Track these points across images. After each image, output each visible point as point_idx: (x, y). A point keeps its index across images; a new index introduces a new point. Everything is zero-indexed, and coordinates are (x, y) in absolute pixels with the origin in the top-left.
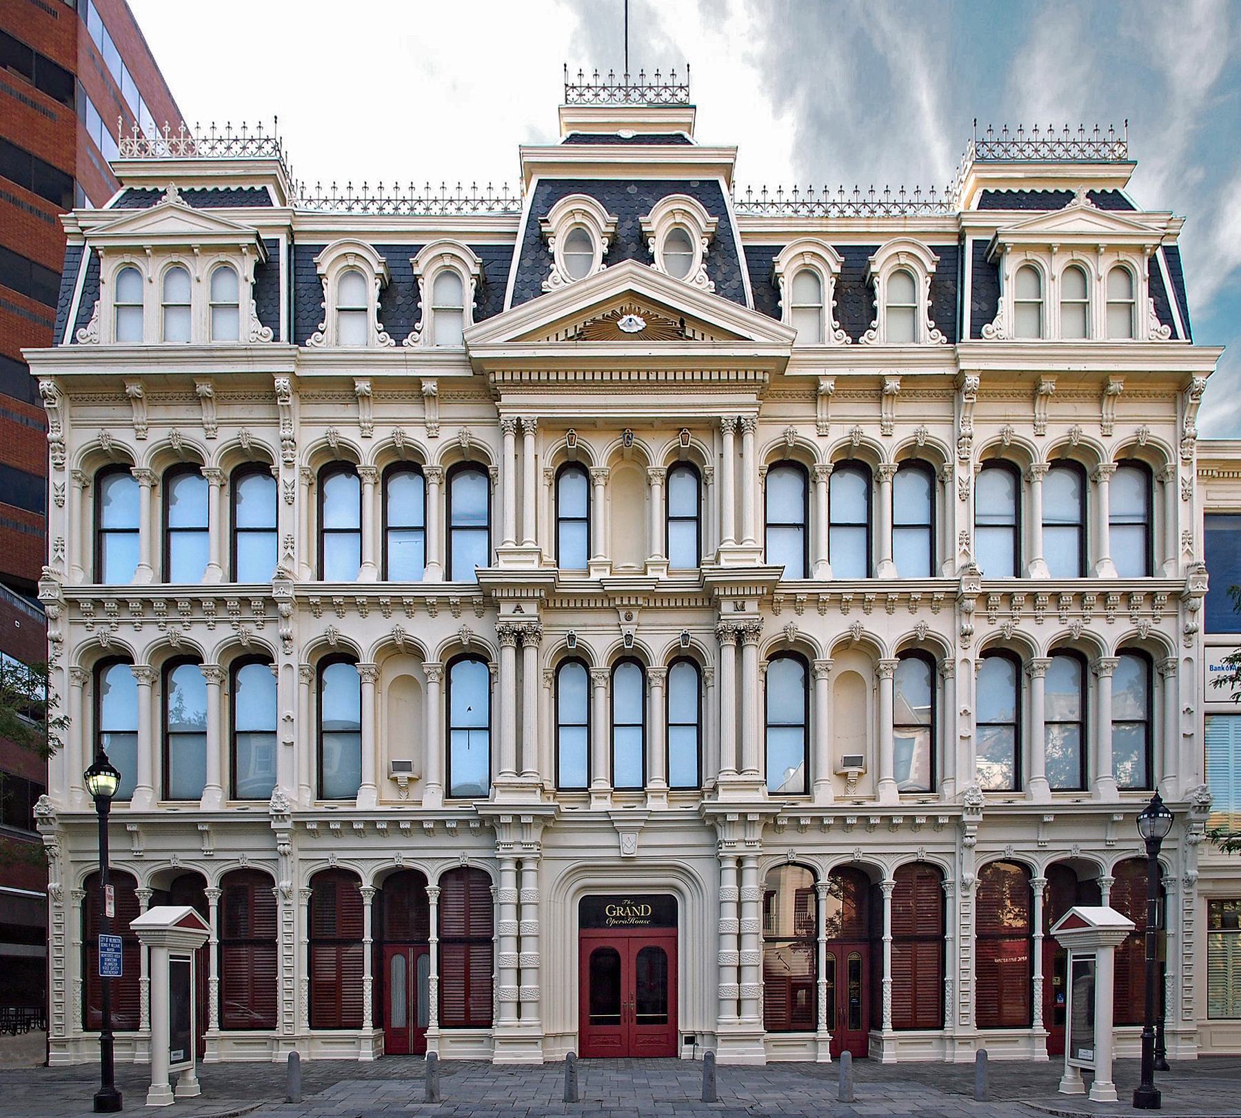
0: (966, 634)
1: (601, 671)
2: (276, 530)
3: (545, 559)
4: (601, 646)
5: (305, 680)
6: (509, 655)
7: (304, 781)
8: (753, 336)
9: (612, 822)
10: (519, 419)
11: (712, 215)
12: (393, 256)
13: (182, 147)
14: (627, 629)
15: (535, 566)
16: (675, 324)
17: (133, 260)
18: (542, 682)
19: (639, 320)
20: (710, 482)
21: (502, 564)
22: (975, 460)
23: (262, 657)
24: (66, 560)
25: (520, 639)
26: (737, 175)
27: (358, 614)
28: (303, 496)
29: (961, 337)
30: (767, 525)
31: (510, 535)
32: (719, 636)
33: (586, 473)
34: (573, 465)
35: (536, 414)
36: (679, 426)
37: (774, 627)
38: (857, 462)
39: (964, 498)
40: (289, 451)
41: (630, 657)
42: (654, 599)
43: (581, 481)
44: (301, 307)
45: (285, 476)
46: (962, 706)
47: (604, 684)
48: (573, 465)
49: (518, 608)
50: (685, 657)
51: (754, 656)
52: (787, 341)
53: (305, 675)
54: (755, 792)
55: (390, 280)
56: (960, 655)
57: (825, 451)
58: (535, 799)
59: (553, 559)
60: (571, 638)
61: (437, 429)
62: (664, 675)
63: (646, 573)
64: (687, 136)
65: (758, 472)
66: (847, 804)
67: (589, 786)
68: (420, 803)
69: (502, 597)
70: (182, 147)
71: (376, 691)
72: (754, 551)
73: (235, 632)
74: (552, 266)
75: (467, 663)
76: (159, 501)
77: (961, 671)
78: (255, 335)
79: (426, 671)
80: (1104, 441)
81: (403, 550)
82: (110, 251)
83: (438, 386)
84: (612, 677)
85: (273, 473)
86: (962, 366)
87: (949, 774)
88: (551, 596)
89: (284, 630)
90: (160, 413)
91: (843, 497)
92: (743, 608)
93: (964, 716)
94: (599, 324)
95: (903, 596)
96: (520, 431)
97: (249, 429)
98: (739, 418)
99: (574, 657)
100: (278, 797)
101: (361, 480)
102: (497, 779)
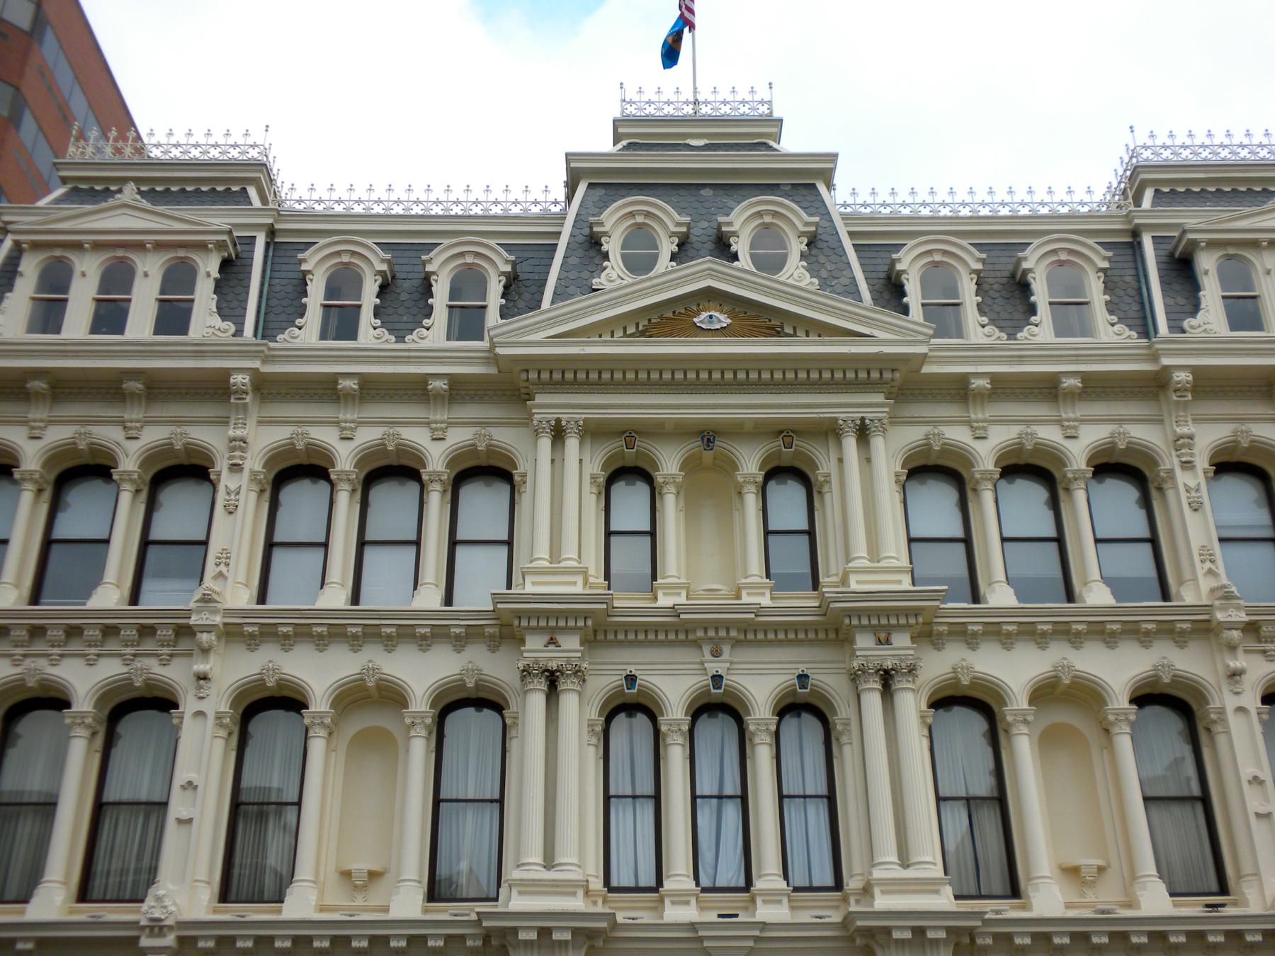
0: (1235, 675)
1: (678, 722)
2: (205, 543)
3: (591, 580)
4: (675, 688)
5: (223, 733)
6: (537, 701)
7: (203, 875)
8: (875, 332)
9: (701, 939)
10: (863, 419)
11: (811, 215)
12: (398, 253)
13: (128, 151)
14: (715, 667)
15: (578, 589)
16: (756, 318)
17: (128, 255)
18: (586, 737)
19: (722, 317)
20: (826, 489)
21: (531, 587)
22: (1202, 462)
23: (163, 703)
24: (230, 576)
25: (553, 680)
26: (838, 179)
27: (245, 647)
28: (251, 508)
29: (1156, 331)
30: (911, 540)
31: (543, 551)
32: (855, 677)
33: (648, 478)
34: (628, 471)
35: (581, 415)
36: (785, 432)
37: (938, 666)
38: (1027, 467)
39: (1196, 507)
40: (237, 453)
41: (719, 707)
42: (751, 632)
43: (642, 489)
44: (274, 302)
45: (227, 481)
46: (1247, 771)
47: (680, 740)
48: (628, 471)
49: (552, 641)
50: (798, 705)
51: (911, 704)
52: (921, 338)
53: (221, 726)
54: (935, 896)
55: (393, 277)
56: (1230, 702)
57: (985, 455)
58: (577, 904)
59: (602, 580)
60: (631, 679)
61: (444, 430)
62: (773, 728)
63: (738, 597)
64: (772, 143)
65: (894, 479)
66: (1088, 914)
67: (660, 882)
68: (386, 909)
69: (528, 628)
70: (128, 151)
71: (329, 750)
72: (898, 570)
73: (125, 669)
74: (605, 264)
75: (470, 712)
76: (142, 508)
77: (1233, 721)
78: (211, 330)
79: (408, 721)
80: (1068, 444)
81: (386, 570)
82: (36, 246)
83: (991, 383)
84: (777, 734)
85: (213, 477)
86: (1166, 361)
87: (1247, 868)
88: (601, 630)
89: (200, 667)
90: (157, 411)
91: (1025, 507)
92: (888, 642)
93: (1255, 787)
94: (671, 317)
95: (991, 628)
96: (558, 434)
97: (942, 428)
98: (863, 419)
99: (631, 705)
100: (159, 899)
101: (332, 485)
102: (511, 873)
